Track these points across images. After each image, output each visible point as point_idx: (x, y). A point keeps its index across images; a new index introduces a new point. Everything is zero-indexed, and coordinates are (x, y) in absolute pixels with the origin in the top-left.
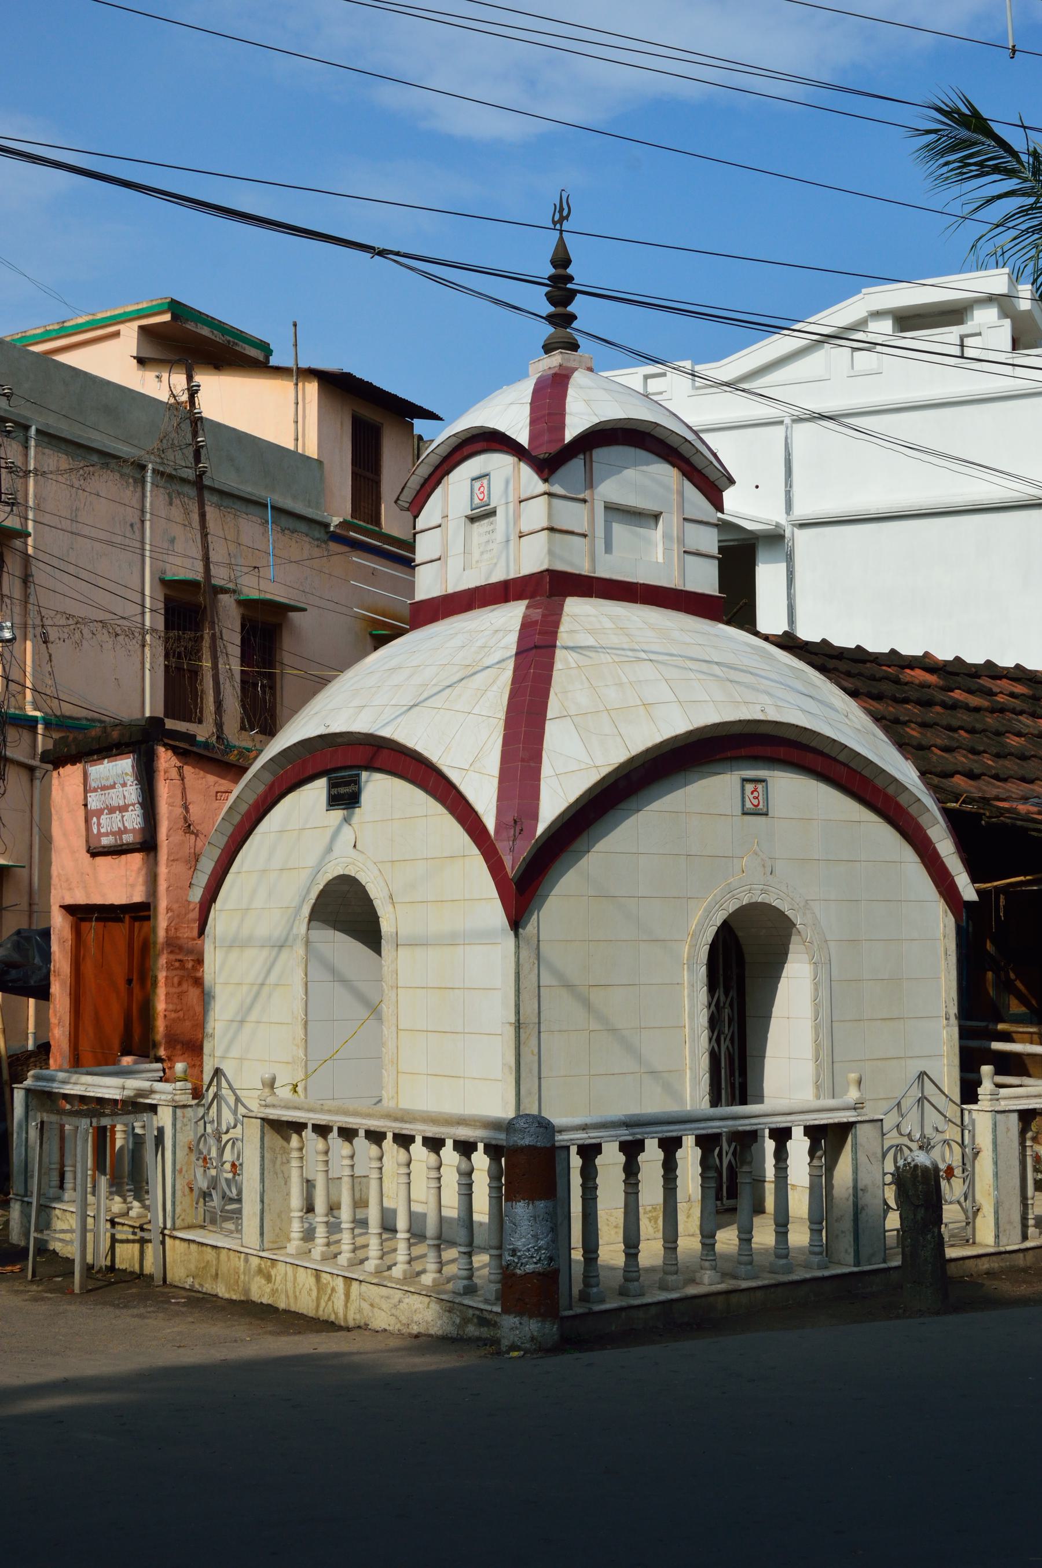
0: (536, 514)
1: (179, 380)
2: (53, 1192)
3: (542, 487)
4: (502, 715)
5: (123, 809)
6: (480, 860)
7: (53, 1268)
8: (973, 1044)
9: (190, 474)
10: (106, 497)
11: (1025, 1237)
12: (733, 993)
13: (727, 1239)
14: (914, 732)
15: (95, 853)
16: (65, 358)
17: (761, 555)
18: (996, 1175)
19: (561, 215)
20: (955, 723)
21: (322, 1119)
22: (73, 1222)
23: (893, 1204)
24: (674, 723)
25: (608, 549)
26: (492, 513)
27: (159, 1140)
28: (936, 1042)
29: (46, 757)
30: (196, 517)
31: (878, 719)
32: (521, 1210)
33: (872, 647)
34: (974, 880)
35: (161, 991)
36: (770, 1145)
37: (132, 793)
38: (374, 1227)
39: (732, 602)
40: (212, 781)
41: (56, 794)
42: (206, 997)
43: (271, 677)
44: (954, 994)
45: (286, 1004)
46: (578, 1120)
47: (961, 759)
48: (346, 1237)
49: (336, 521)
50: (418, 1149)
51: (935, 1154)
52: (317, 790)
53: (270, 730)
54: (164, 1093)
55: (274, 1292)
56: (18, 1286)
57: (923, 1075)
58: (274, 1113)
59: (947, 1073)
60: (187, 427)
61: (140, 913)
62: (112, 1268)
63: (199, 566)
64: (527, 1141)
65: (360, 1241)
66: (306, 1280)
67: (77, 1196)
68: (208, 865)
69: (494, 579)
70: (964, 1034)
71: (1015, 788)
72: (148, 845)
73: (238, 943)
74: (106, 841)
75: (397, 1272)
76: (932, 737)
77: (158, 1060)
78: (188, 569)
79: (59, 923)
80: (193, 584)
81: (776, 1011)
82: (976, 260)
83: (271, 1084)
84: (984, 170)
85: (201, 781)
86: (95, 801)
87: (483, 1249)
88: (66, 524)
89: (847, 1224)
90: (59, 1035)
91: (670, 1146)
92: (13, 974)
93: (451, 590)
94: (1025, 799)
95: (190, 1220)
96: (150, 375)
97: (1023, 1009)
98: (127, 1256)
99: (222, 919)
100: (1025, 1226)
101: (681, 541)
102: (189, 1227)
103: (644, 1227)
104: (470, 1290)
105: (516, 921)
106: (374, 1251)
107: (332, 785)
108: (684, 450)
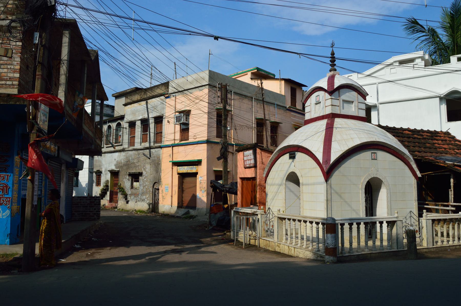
0: (329, 102)
1: (259, 82)
2: (239, 230)
3: (330, 97)
4: (323, 141)
5: (251, 160)
6: (319, 168)
7: (239, 244)
8: (421, 206)
9: (261, 99)
10: (246, 104)
11: (433, 245)
12: (370, 195)
13: (370, 243)
14: (406, 143)
15: (245, 168)
16: (238, 79)
17: (372, 110)
18: (427, 232)
19: (332, 46)
20: (415, 141)
21: (289, 217)
22: (243, 235)
23: (404, 237)
24: (357, 142)
25: (343, 109)
26: (320, 103)
27: (258, 221)
28: (414, 206)
29: (236, 151)
30: (262, 107)
31: (399, 141)
32: (329, 235)
33: (397, 127)
34: (420, 173)
35: (258, 193)
36: (340, 227)
37: (252, 157)
38: (299, 238)
39: (368, 119)
40: (267, 154)
41: (238, 157)
42: (266, 195)
43: (276, 136)
44: (416, 196)
45: (282, 195)
46: (340, 219)
47: (417, 148)
48: (294, 240)
49: (288, 106)
50: (308, 223)
51: (414, 227)
52: (287, 156)
53: (277, 146)
54: (259, 212)
55: (280, 250)
56: (233, 246)
57: (411, 211)
58: (280, 216)
59: (416, 211)
60: (261, 90)
61: (254, 179)
62: (250, 244)
63: (263, 115)
64: (330, 222)
65: (297, 241)
66: (286, 248)
67: (244, 231)
68: (266, 170)
69: (321, 115)
70: (419, 204)
71: (429, 154)
72: (255, 166)
73: (272, 185)
74: (247, 166)
75: (304, 247)
76: (410, 144)
77: (257, 206)
78: (261, 116)
79: (239, 181)
80: (262, 119)
81: (379, 199)
82: (417, 49)
83: (279, 211)
84: (418, 31)
85: (265, 155)
86: (245, 159)
87: (321, 243)
88: (239, 108)
89: (395, 241)
90: (239, 201)
91: (358, 224)
92: (231, 190)
93: (312, 118)
94: (431, 156)
95: (264, 236)
96: (253, 81)
97: (431, 199)
98: (252, 242)
99: (269, 180)
100: (433, 243)
101: (358, 107)
102: (264, 237)
103: (353, 240)
104: (319, 251)
105: (327, 180)
106: (299, 242)
107: (290, 155)
108: (358, 89)
